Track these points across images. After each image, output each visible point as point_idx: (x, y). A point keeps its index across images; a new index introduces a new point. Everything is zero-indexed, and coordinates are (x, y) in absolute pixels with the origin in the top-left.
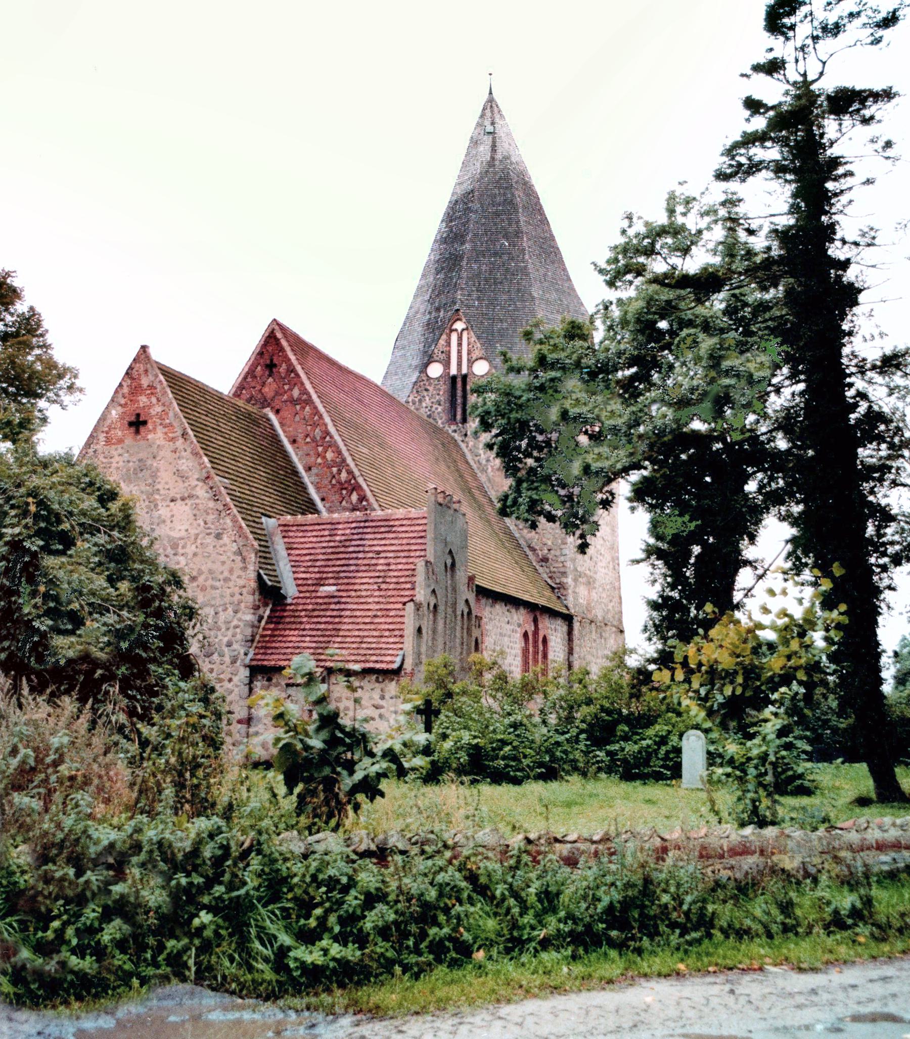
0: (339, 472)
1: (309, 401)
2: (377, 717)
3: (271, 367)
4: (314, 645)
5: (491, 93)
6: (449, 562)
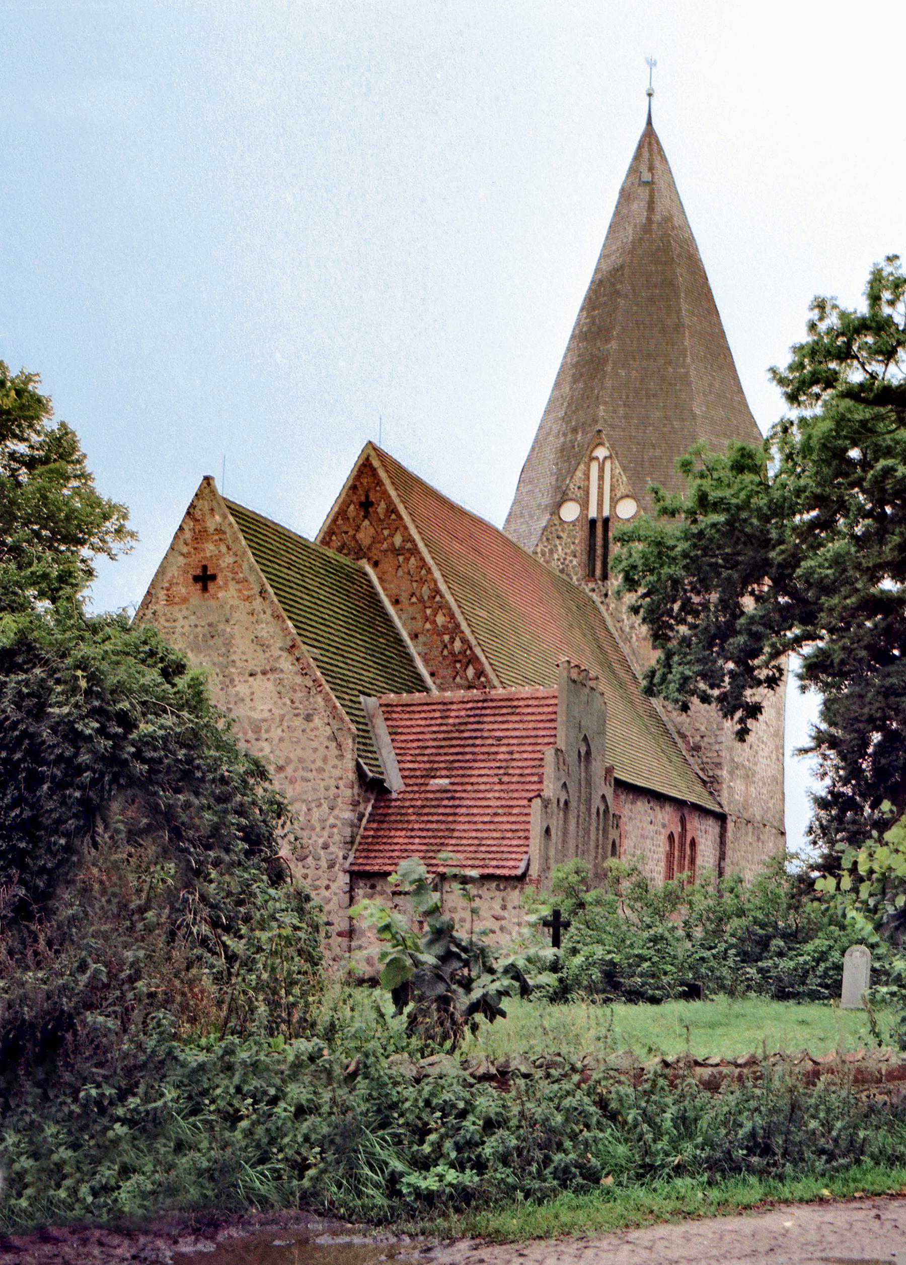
0: (452, 640)
1: (415, 551)
2: (497, 930)
3: (366, 506)
4: (424, 848)
5: (649, 122)
6: (583, 750)
